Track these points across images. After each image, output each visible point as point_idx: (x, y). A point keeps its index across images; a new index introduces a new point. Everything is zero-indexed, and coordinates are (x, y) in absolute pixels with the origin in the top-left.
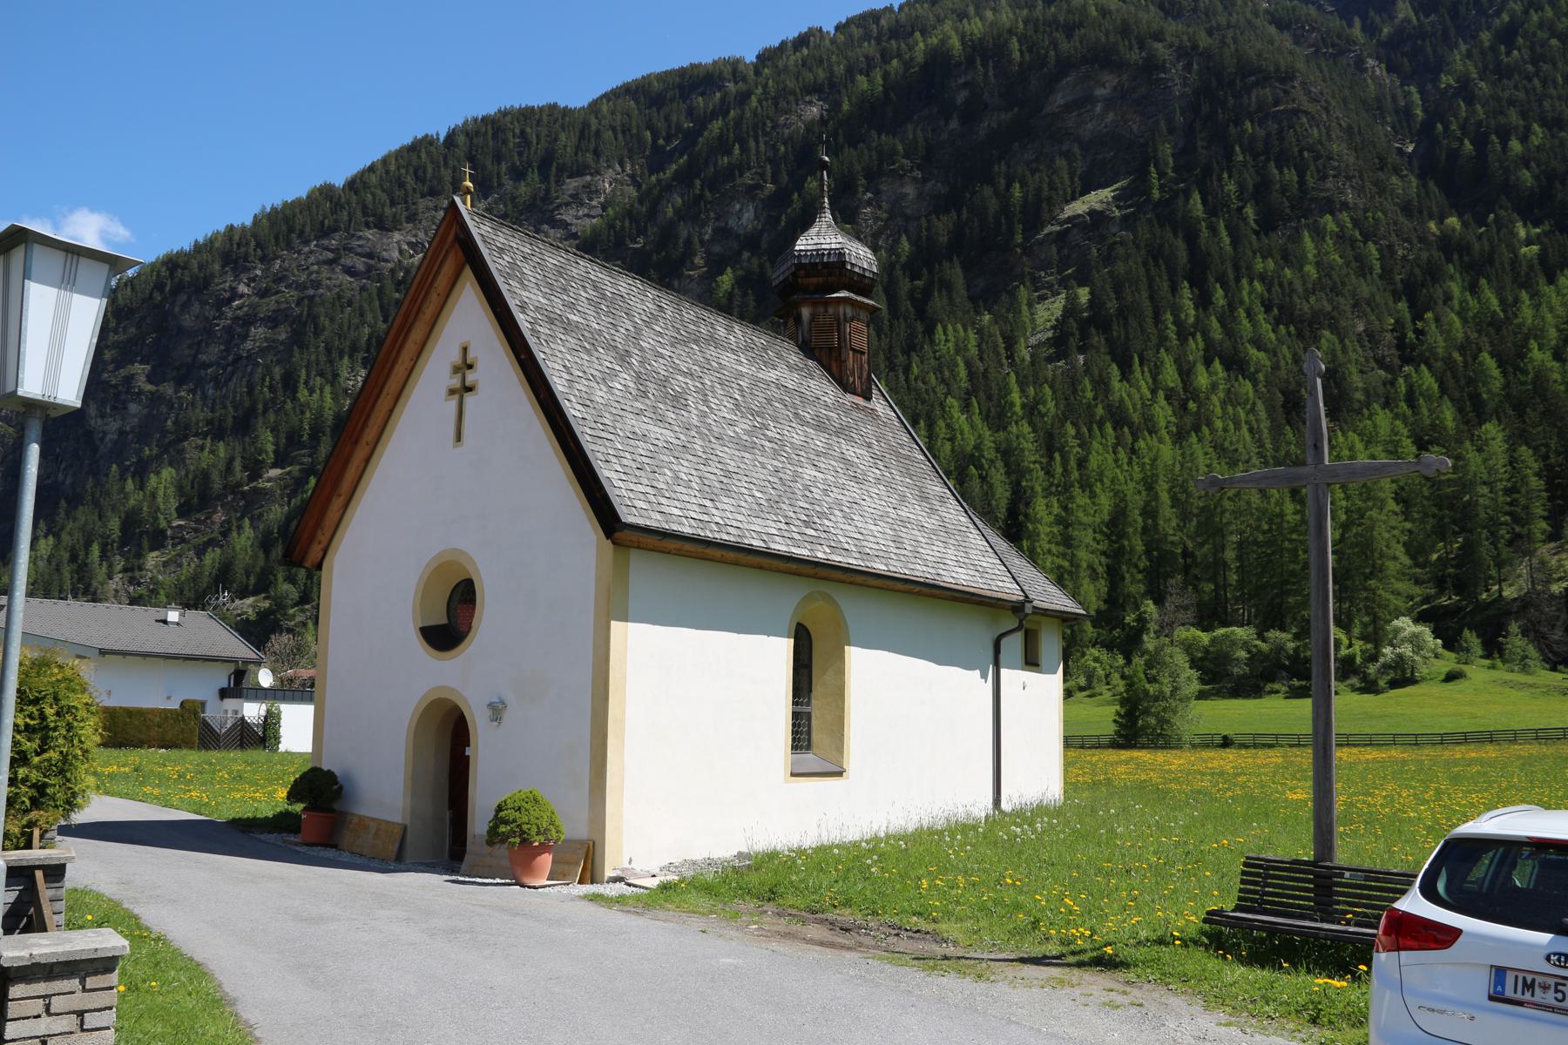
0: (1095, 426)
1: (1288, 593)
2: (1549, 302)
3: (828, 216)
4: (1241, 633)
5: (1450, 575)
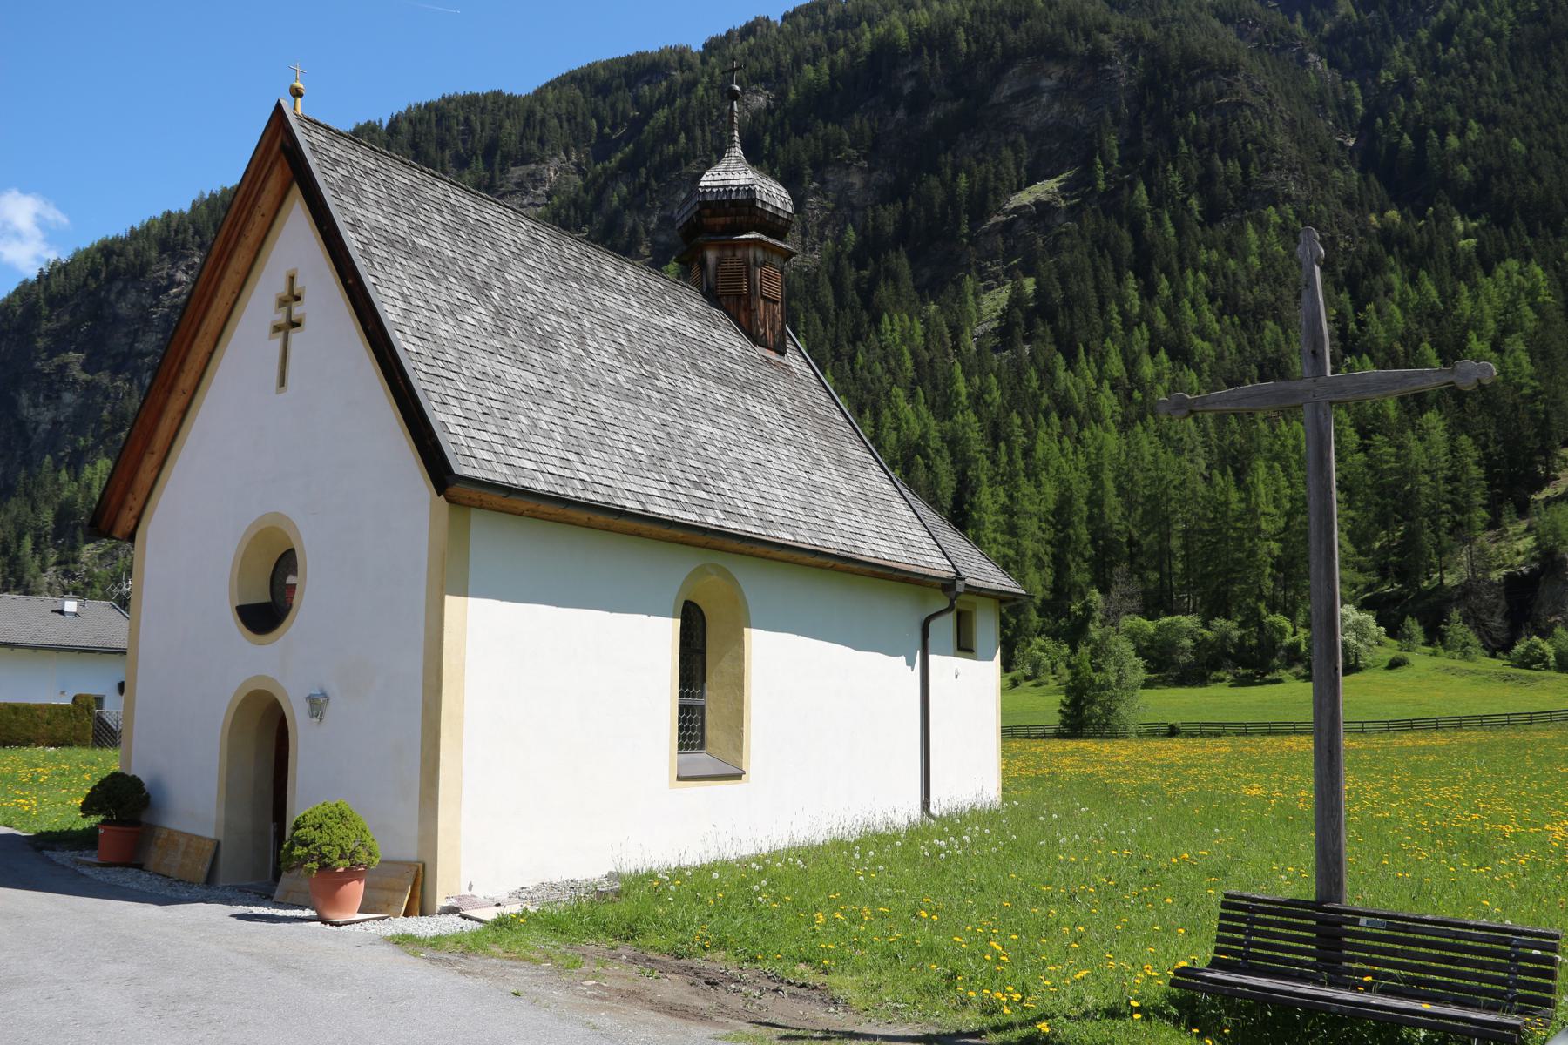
0: (1041, 415)
1: (1233, 582)
2: (1486, 294)
3: (738, 151)
4: (1187, 621)
5: (1392, 562)
